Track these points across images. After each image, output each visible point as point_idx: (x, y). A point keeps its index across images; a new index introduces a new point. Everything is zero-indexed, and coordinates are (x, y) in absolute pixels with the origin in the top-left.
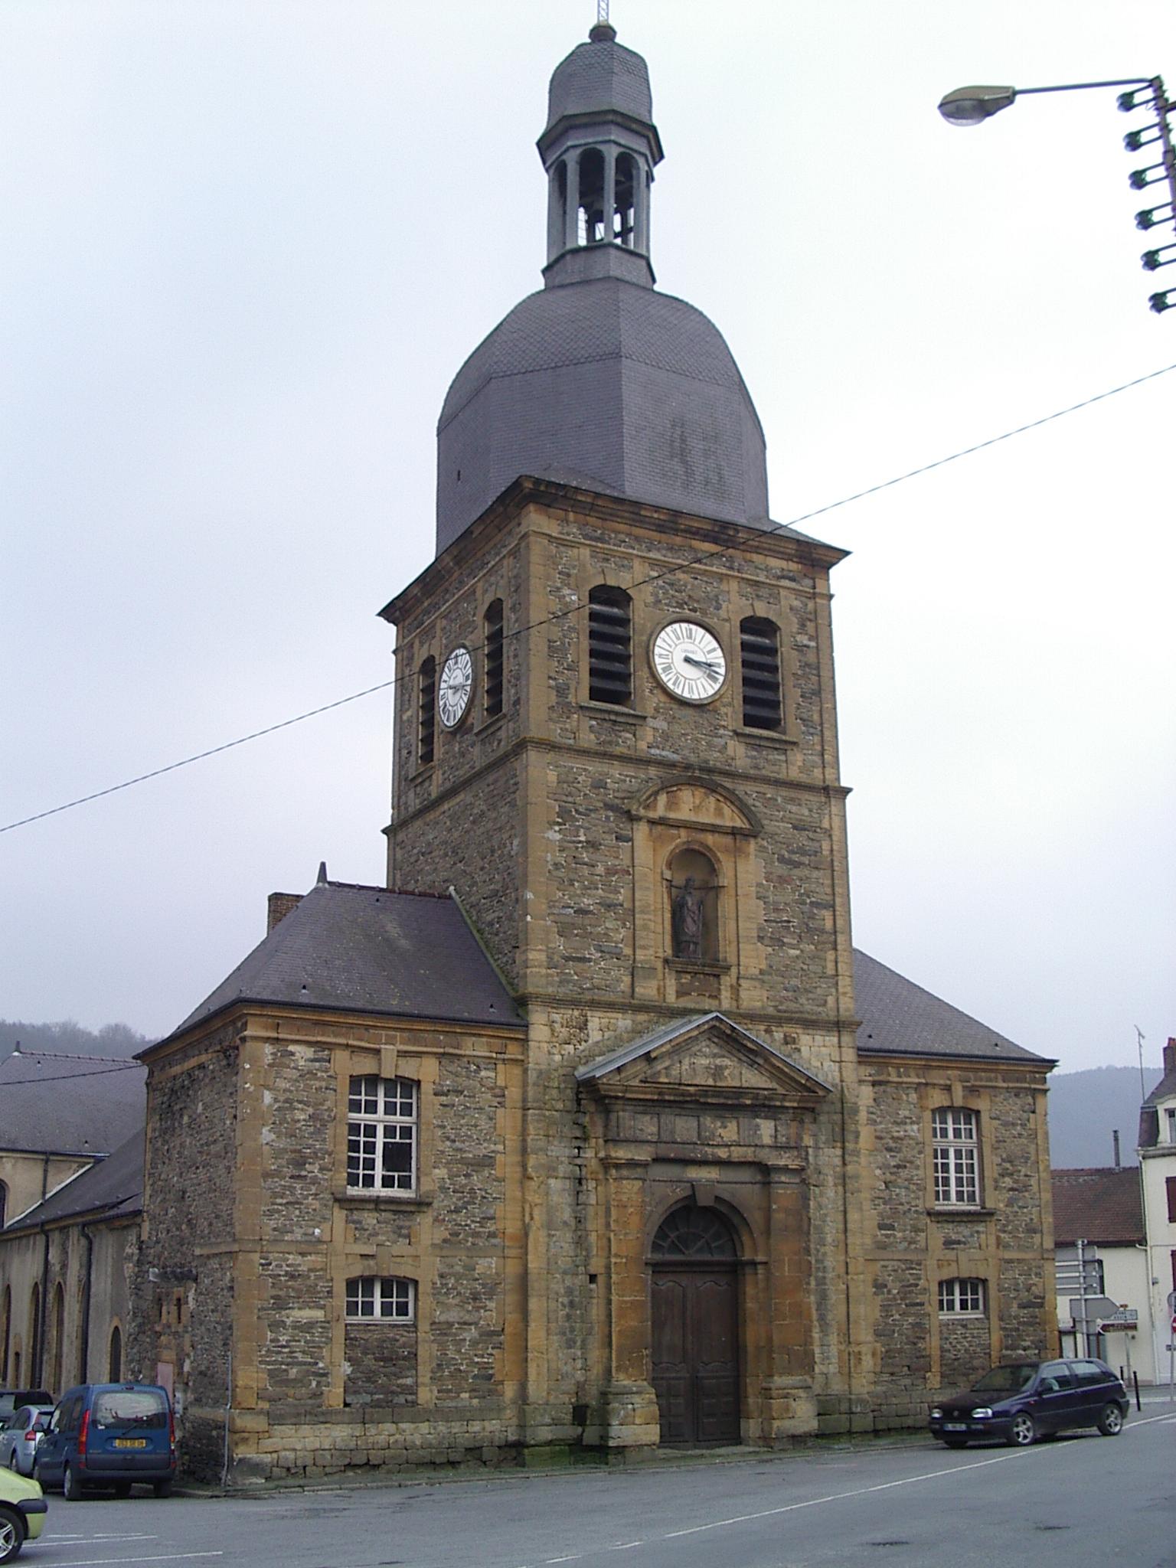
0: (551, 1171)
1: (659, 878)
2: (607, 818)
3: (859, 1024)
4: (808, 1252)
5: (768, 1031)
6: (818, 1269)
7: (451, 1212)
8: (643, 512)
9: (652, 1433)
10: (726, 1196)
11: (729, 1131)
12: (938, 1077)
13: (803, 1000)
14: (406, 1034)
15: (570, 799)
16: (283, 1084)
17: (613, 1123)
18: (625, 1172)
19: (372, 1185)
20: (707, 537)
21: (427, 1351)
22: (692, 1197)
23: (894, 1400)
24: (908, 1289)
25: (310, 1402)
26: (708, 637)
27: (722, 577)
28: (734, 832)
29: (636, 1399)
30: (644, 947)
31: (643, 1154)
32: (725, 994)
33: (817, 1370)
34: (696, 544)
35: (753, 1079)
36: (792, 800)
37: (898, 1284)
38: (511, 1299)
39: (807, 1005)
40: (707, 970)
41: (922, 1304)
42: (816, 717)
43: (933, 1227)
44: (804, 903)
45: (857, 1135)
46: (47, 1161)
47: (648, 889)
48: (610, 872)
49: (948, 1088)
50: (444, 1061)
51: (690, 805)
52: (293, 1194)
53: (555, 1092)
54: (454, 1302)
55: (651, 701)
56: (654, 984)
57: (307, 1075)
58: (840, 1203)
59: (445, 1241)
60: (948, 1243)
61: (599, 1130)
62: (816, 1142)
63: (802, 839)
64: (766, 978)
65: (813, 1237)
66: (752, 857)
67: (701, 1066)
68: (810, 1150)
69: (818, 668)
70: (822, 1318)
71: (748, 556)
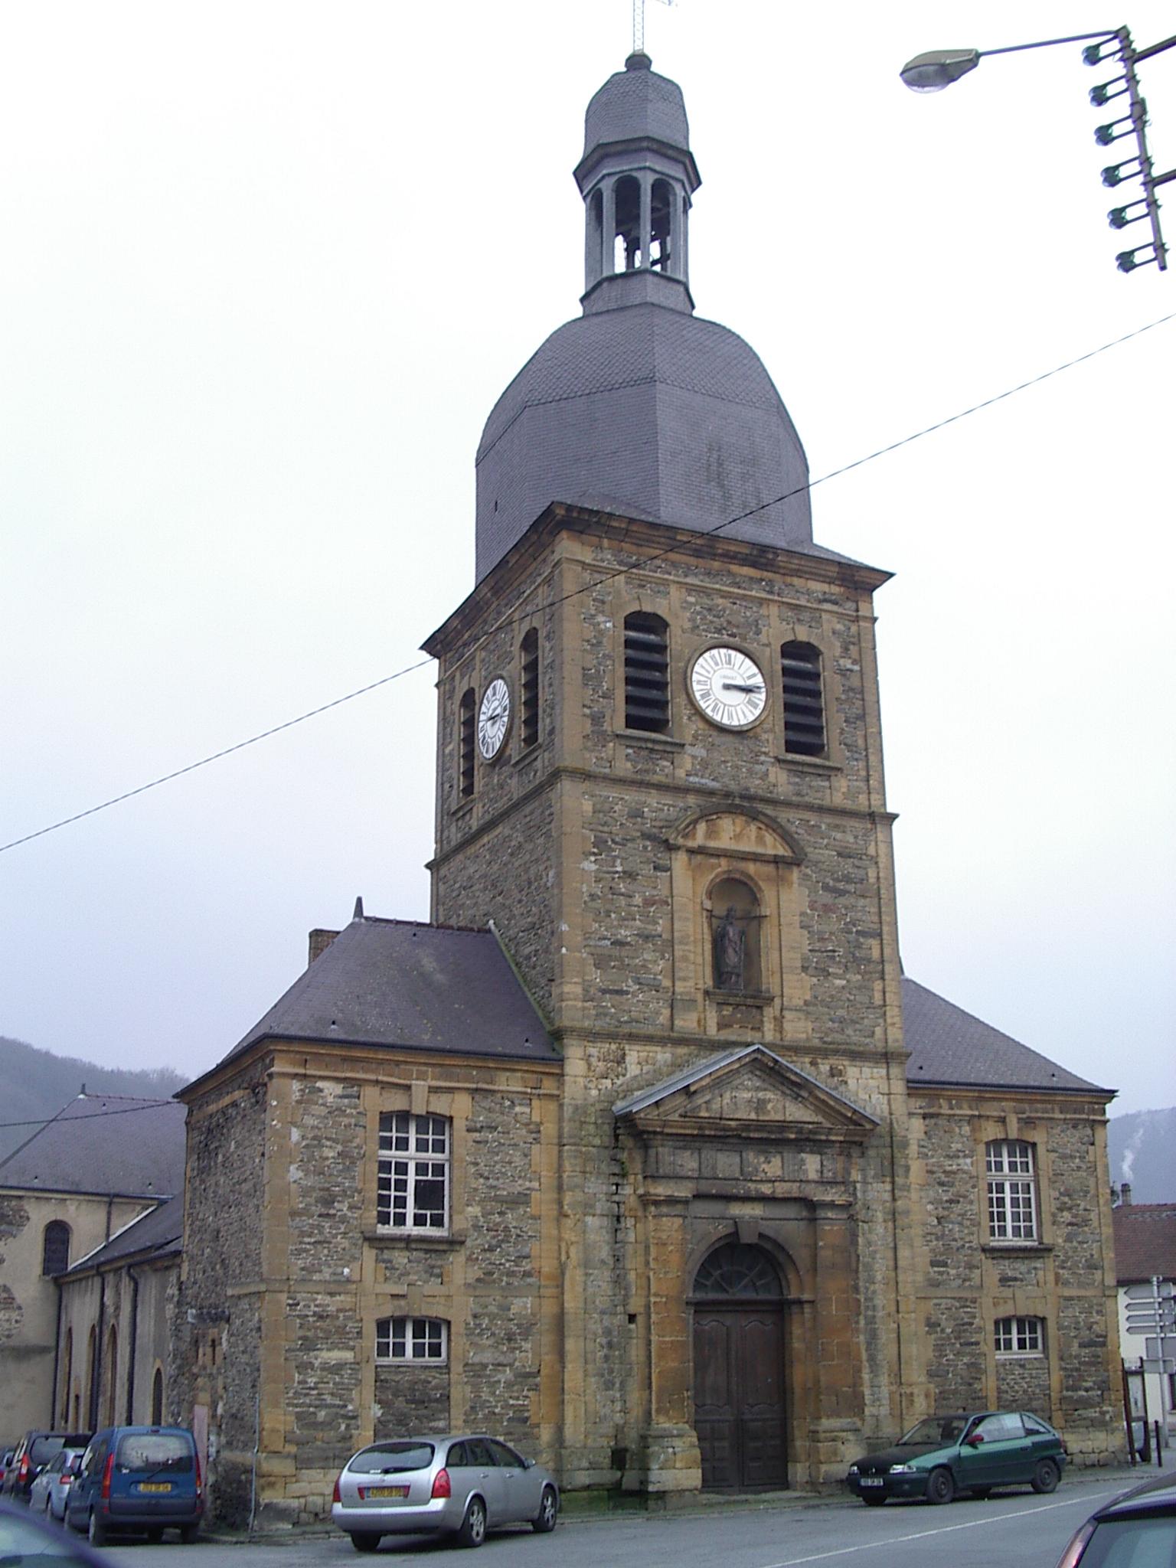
0: (587, 1207)
2: (645, 847)
3: (908, 1055)
4: (856, 1289)
5: (813, 1063)
7: (484, 1250)
9: (693, 1478)
10: (771, 1233)
11: (773, 1166)
12: (992, 1110)
13: (850, 1032)
14: (438, 1070)
15: (606, 829)
16: (310, 1121)
17: (652, 1159)
18: (664, 1209)
19: (404, 1224)
21: (460, 1394)
22: (735, 1234)
25: (340, 1445)
26: (748, 661)
27: (761, 602)
28: (776, 860)
29: (677, 1442)
30: (685, 979)
31: (683, 1191)
32: (769, 1027)
33: (866, 1410)
34: (734, 568)
35: (796, 1112)
36: (837, 826)
38: (547, 1339)
39: (853, 1036)
40: (749, 1001)
41: (977, 1343)
42: (861, 742)
43: (988, 1263)
44: (850, 932)
45: (907, 1169)
46: (110, 1204)
47: (687, 919)
48: (648, 902)
49: (1003, 1120)
50: (477, 1097)
51: (731, 834)
52: (321, 1233)
53: (592, 1129)
55: (686, 729)
56: (694, 1016)
57: (337, 1111)
58: (890, 1239)
59: (478, 1280)
60: (1004, 1280)
61: (638, 1167)
62: (865, 1177)
63: (848, 867)
64: (811, 1009)
65: (862, 1275)
66: (795, 885)
67: (744, 1099)
68: (858, 1186)
69: (862, 692)
70: (872, 1359)
71: (789, 579)
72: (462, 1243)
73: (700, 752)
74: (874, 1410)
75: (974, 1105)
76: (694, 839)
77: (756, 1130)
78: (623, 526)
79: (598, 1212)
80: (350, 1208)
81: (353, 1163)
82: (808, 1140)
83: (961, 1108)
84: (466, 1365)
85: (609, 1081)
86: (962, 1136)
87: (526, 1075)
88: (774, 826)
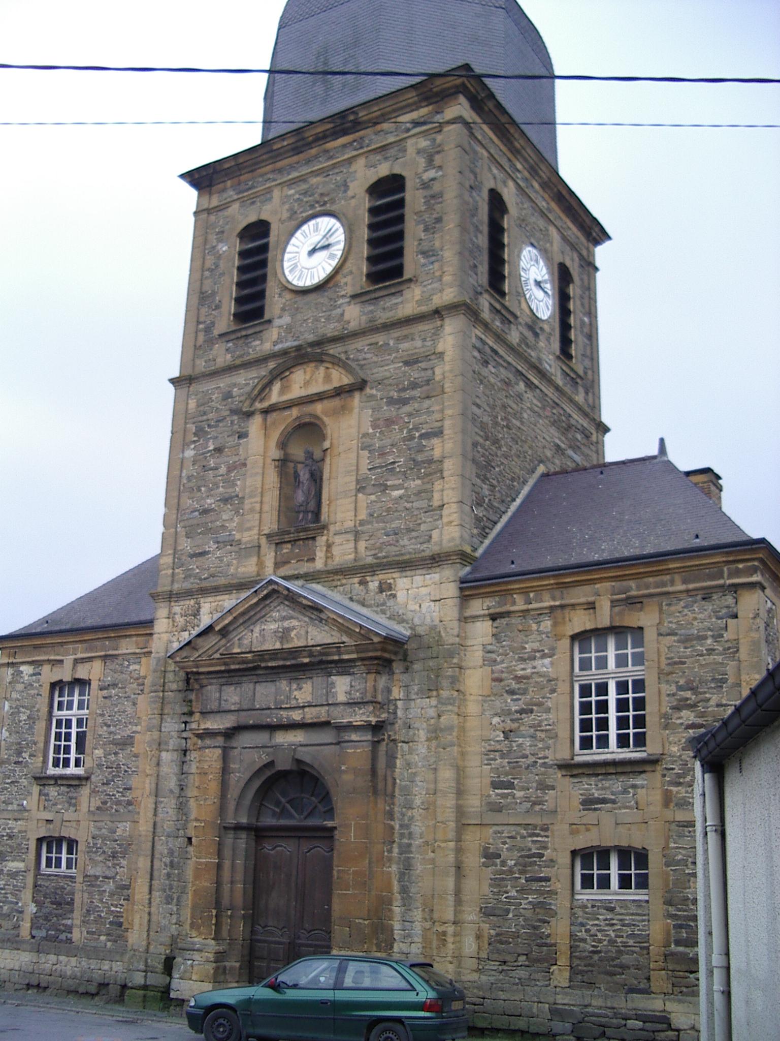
1: (269, 461)
4: (391, 815)
5: (363, 583)
6: (402, 836)
8: (275, 147)
10: (307, 759)
11: (304, 692)
12: (580, 595)
13: (405, 542)
14: (85, 645)
16: (15, 695)
18: (208, 742)
19: (69, 766)
20: (336, 134)
23: (502, 995)
24: (529, 859)
25: (12, 932)
28: (339, 392)
29: (197, 956)
32: (320, 554)
33: (395, 945)
35: (320, 636)
36: (406, 337)
37: (516, 854)
39: (409, 546)
40: (302, 535)
41: (547, 879)
44: (412, 438)
48: (230, 470)
49: (591, 606)
52: (14, 775)
54: (100, 859)
59: (98, 808)
60: (589, 803)
62: (408, 693)
63: (415, 374)
65: (399, 799)
66: (356, 411)
67: (264, 635)
68: (399, 703)
70: (404, 890)
71: (378, 127)
72: (87, 779)
73: (287, 319)
74: (404, 948)
75: (557, 593)
76: (270, 397)
77: (271, 659)
78: (233, 164)
79: (171, 748)
80: (30, 756)
81: (34, 723)
82: (321, 662)
83: (541, 601)
84: (87, 876)
85: (187, 633)
86: (540, 633)
87: (140, 639)
88: (337, 362)
